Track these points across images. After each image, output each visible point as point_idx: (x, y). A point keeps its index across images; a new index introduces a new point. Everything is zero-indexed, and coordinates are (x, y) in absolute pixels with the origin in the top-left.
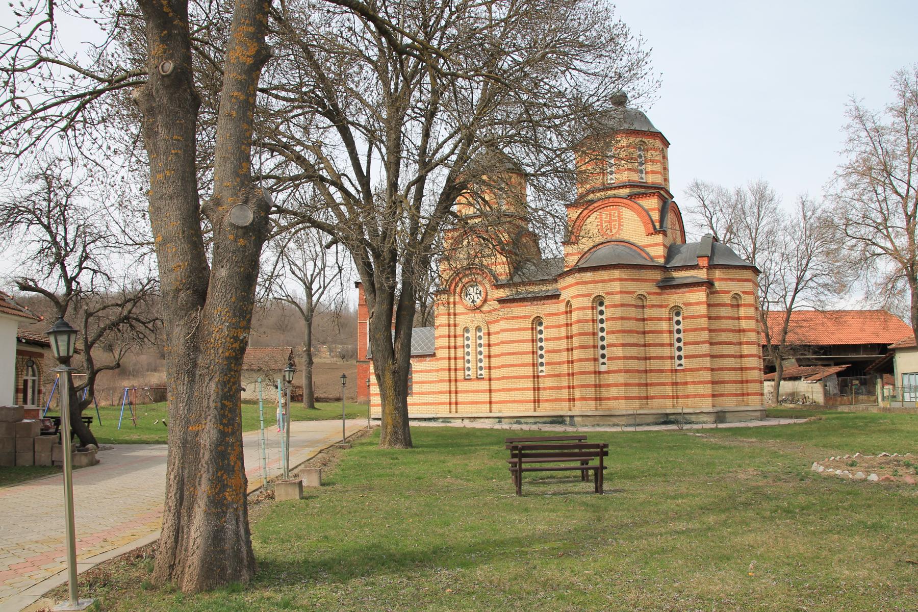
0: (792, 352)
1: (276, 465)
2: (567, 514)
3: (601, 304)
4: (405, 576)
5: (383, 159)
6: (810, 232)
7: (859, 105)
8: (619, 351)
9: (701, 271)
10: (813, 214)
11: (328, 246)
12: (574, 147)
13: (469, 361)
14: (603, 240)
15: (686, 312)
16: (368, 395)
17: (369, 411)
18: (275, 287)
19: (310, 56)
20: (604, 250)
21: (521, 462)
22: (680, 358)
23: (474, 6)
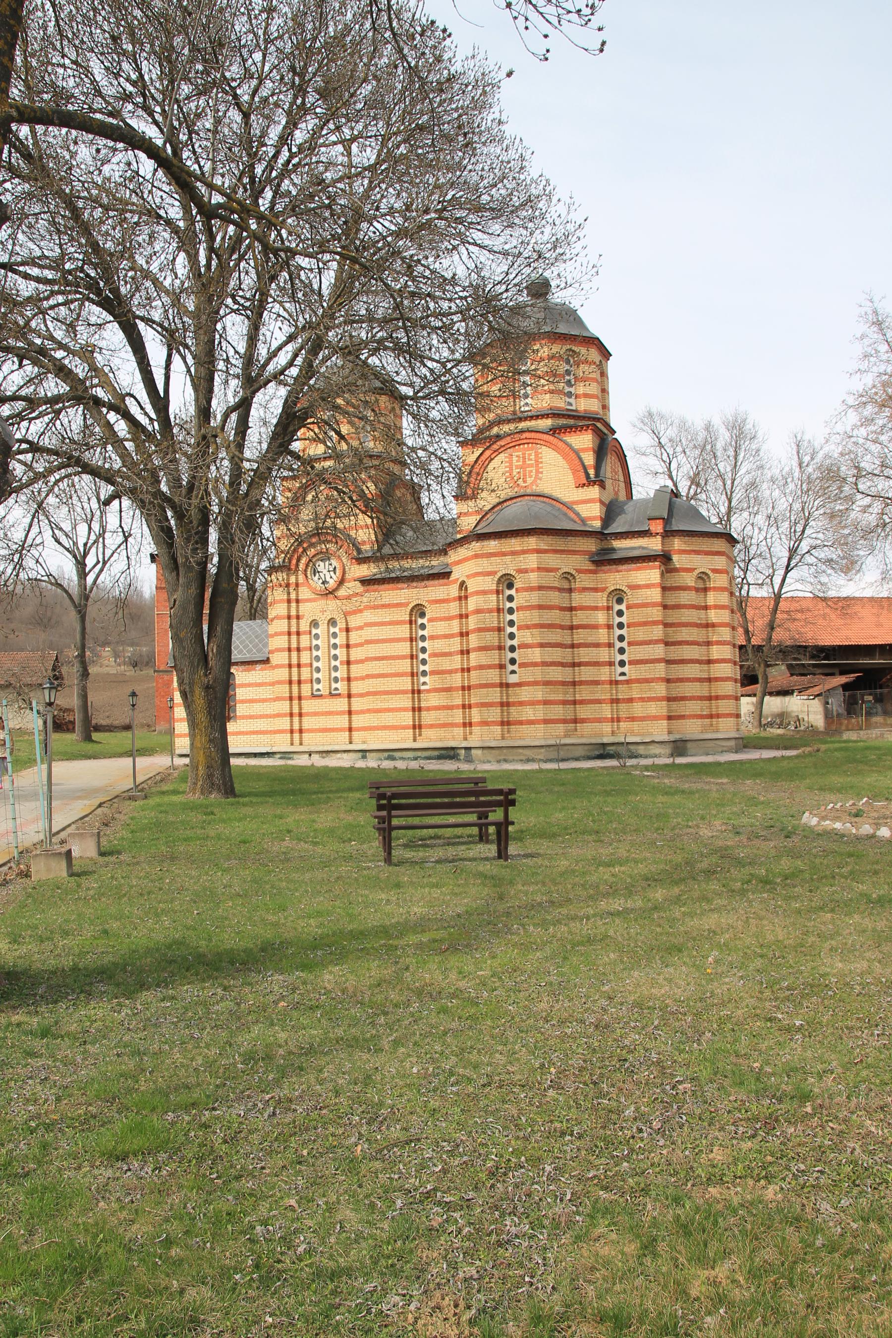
0: (781, 655)
1: (33, 828)
2: (456, 890)
3: (510, 586)
4: (220, 985)
5: (189, 371)
6: (808, 486)
7: (879, 306)
8: (536, 655)
9: (653, 539)
10: (812, 459)
11: (107, 503)
12: (471, 358)
13: (318, 670)
14: (512, 494)
15: (631, 597)
16: (171, 720)
17: (172, 744)
18: (29, 562)
19: (76, 214)
20: (514, 508)
21: (390, 817)
22: (622, 663)
23: (327, 146)
